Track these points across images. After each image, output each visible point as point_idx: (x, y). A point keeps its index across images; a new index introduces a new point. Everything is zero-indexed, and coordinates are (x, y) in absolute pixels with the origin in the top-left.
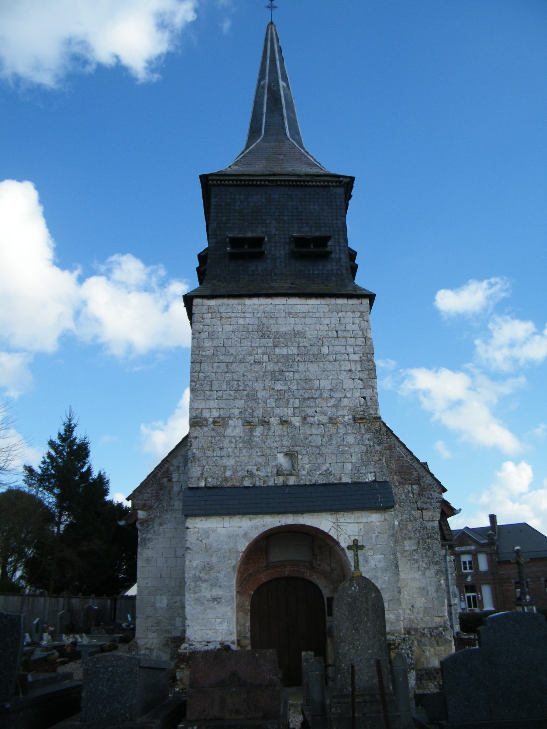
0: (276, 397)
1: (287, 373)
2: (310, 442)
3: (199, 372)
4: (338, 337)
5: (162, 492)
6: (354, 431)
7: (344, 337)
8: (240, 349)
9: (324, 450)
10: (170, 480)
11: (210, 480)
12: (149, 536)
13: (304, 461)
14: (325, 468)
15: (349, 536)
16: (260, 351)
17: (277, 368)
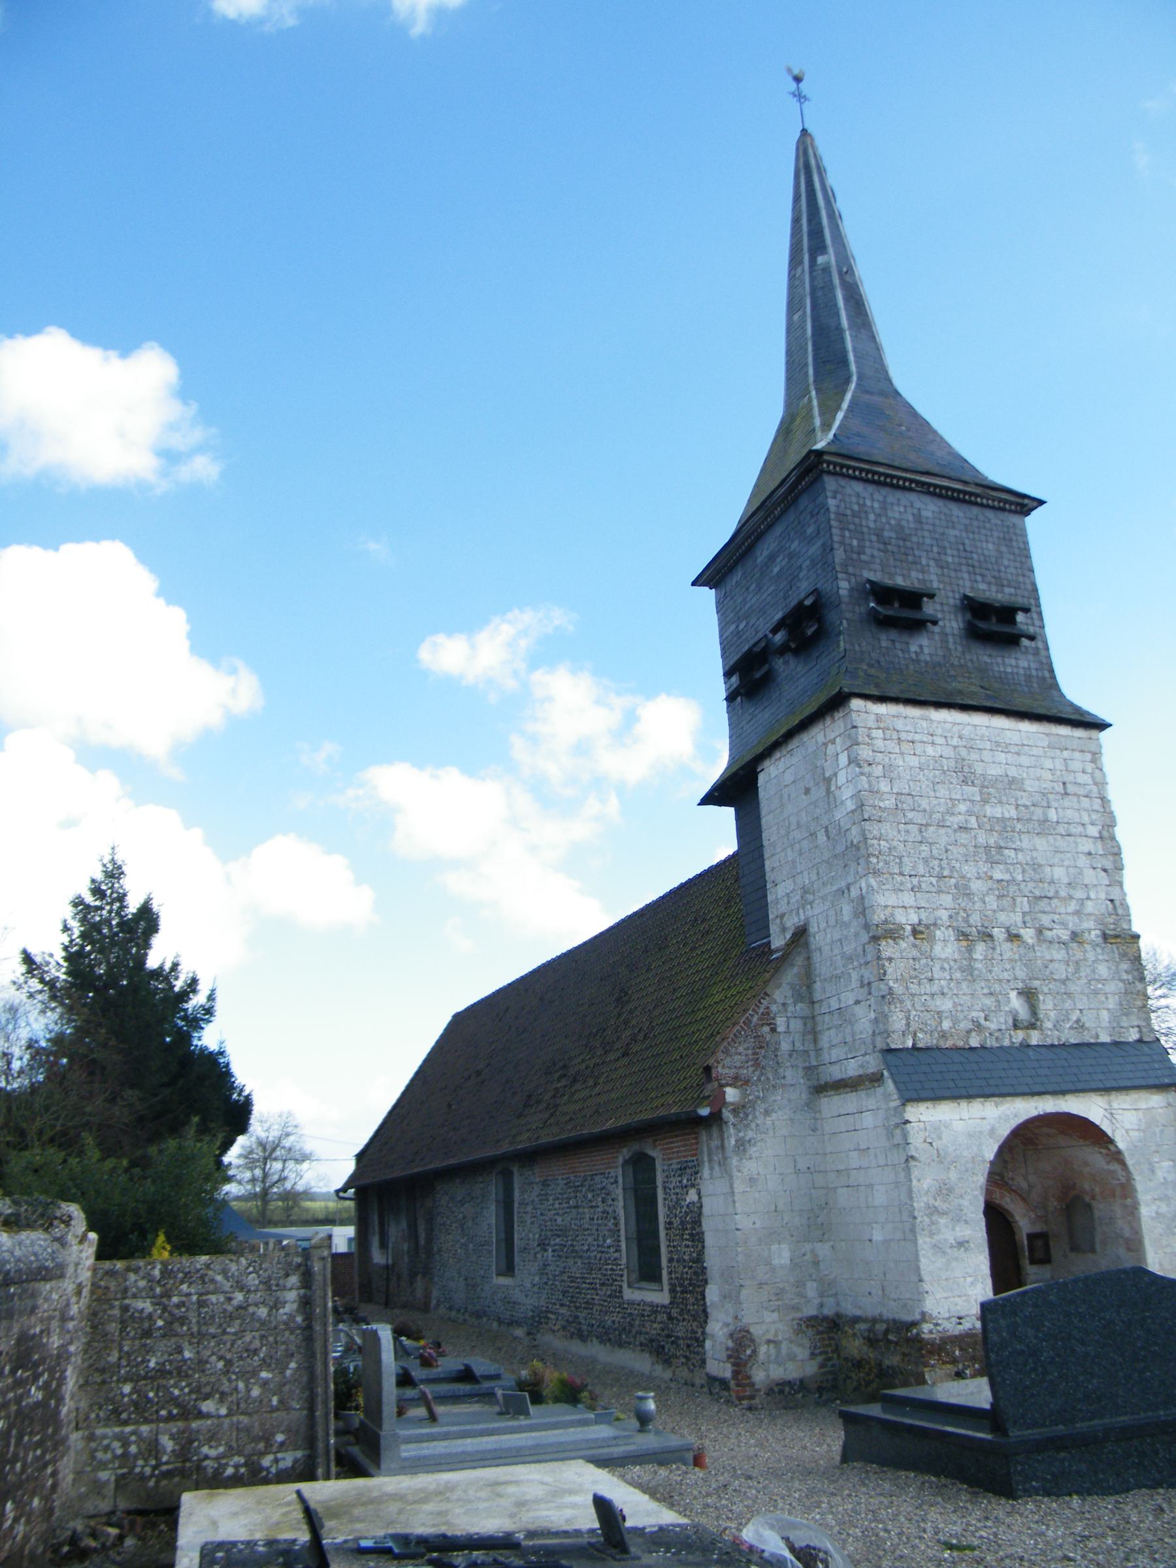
0: (997, 893)
1: (1006, 852)
2: (1052, 973)
3: (879, 840)
4: (1066, 794)
5: (763, 1051)
6: (1106, 957)
7: (1075, 794)
8: (935, 802)
9: (1072, 987)
10: (773, 1030)
11: (920, 1035)
12: (750, 1134)
13: (1046, 1005)
14: (1075, 1018)
15: (1127, 1131)
16: (962, 808)
17: (992, 842)
